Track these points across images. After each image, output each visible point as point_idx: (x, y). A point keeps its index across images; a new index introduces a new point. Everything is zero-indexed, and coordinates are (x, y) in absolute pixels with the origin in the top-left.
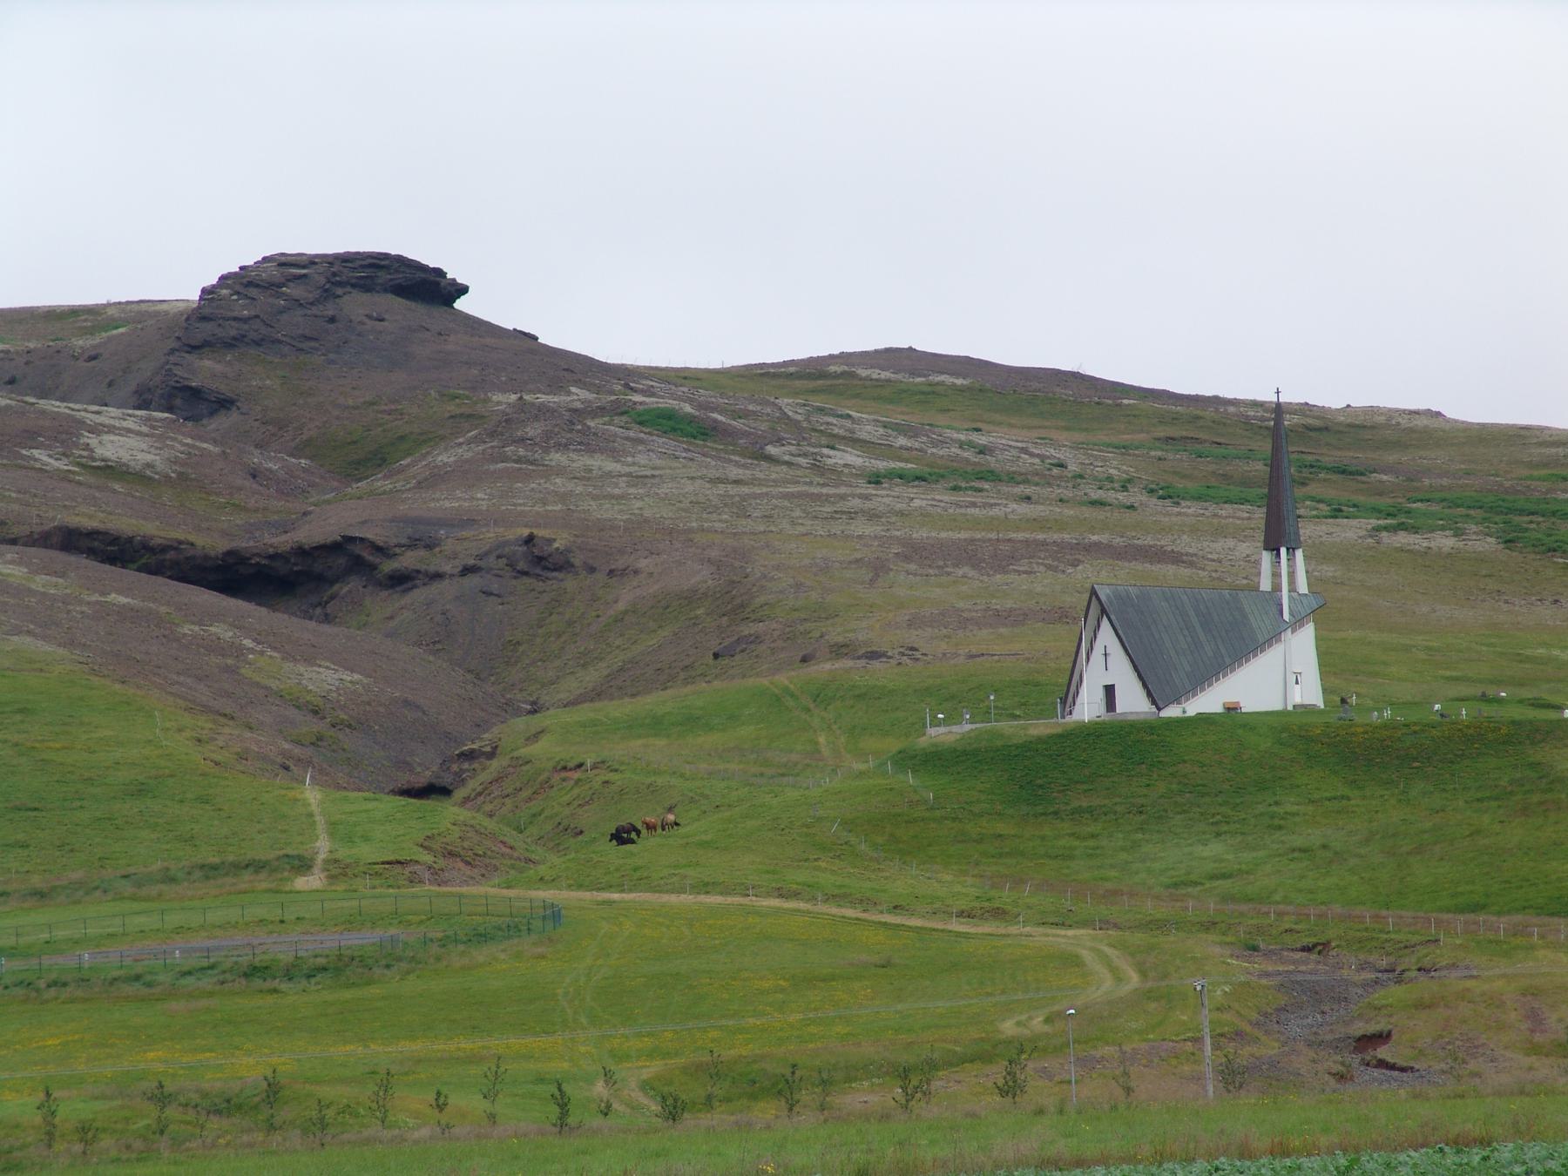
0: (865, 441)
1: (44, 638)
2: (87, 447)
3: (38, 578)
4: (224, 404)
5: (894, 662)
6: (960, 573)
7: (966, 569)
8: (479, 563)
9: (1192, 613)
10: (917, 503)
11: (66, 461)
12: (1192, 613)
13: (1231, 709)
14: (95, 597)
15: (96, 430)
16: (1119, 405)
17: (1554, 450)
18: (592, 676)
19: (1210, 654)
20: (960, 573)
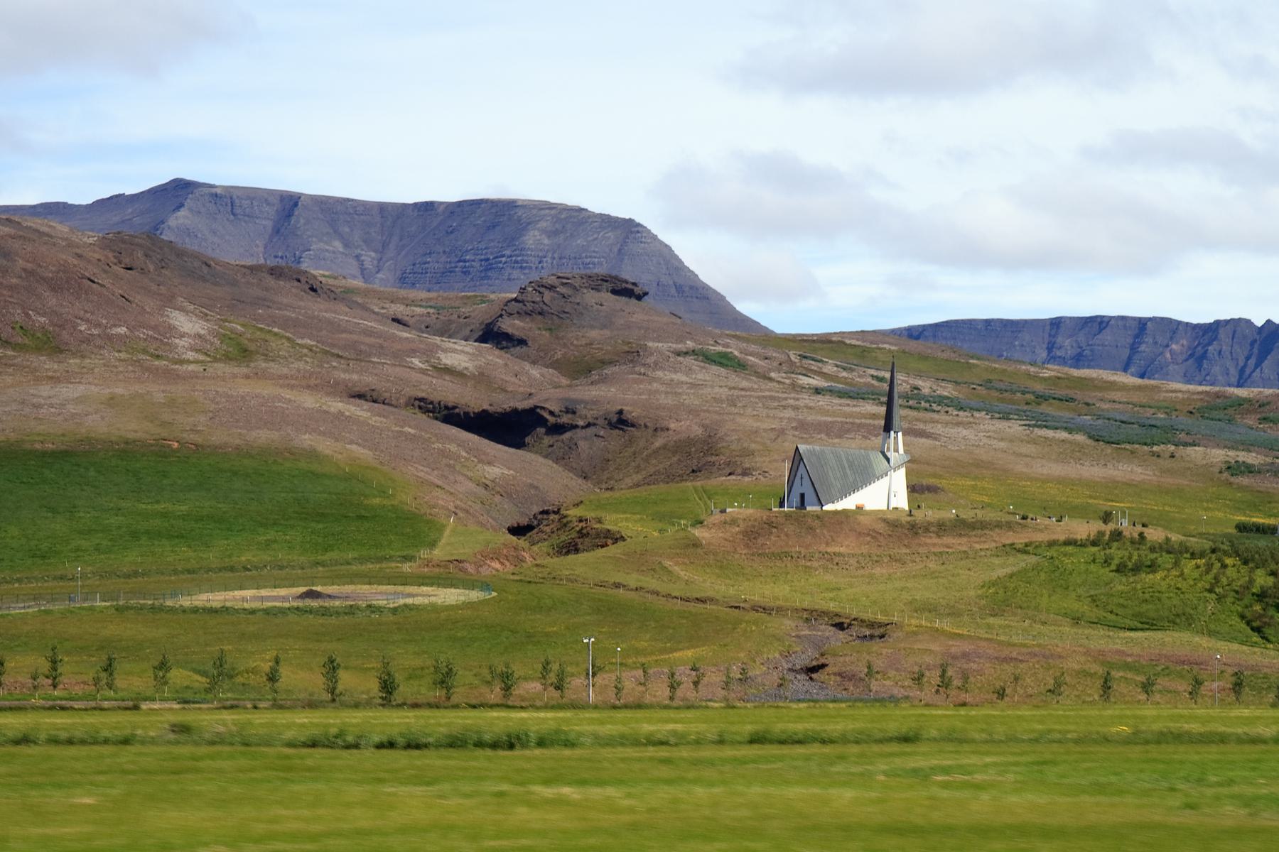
0: (825, 374)
1: (364, 447)
2: (439, 358)
3: (374, 419)
4: (522, 342)
5: (754, 478)
6: (819, 437)
7: (823, 436)
8: (595, 421)
9: (845, 462)
10: (821, 403)
11: (426, 364)
12: (845, 462)
13: (860, 508)
14: (397, 429)
15: (445, 351)
16: (967, 363)
17: (1174, 395)
18: (638, 478)
19: (851, 480)
20: (819, 437)
